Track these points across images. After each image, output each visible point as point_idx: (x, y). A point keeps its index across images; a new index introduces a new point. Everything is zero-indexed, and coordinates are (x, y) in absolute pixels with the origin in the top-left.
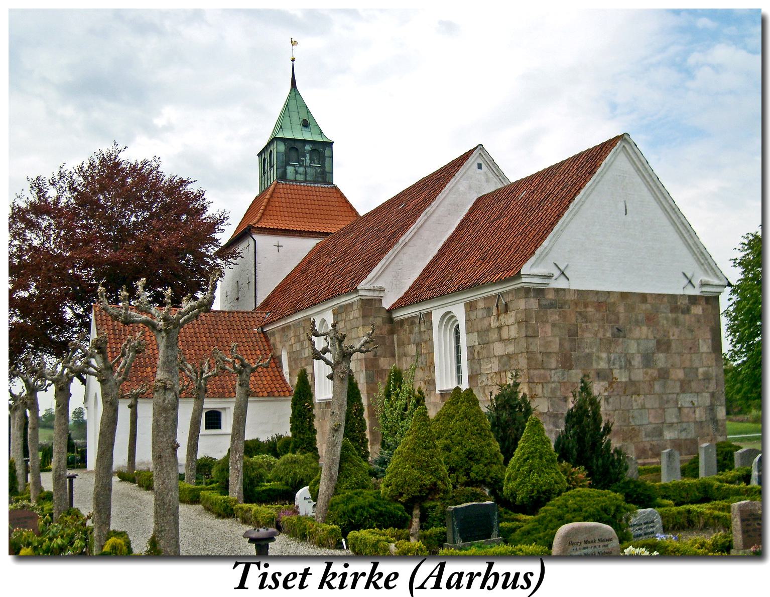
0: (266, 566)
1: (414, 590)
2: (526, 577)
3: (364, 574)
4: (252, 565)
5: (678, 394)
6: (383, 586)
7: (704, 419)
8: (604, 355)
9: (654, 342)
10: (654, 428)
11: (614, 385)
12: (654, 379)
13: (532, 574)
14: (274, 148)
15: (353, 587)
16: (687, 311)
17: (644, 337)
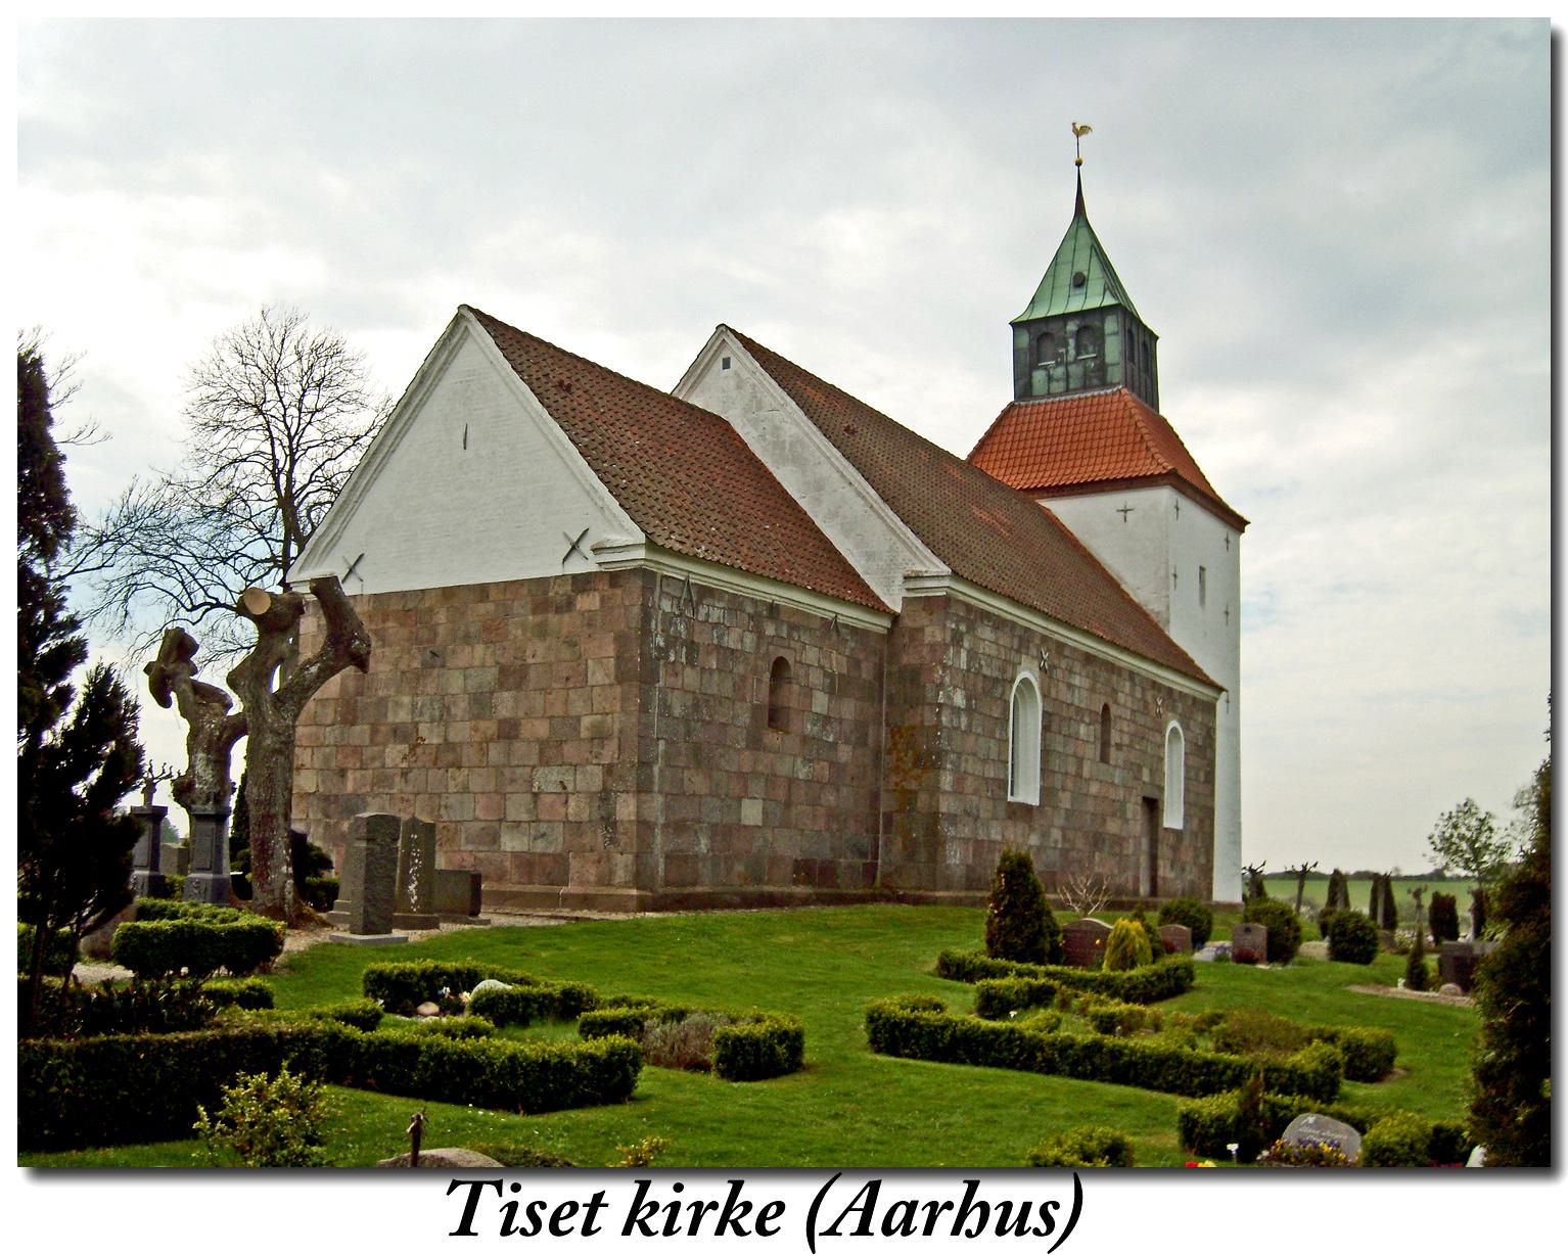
0: (516, 1188)
1: (817, 1238)
2: (1044, 1211)
3: (714, 1205)
4: (485, 1186)
5: (534, 767)
6: (753, 1229)
7: (585, 817)
8: (406, 700)
9: (495, 670)
10: (483, 829)
11: (419, 751)
12: (488, 740)
13: (1056, 1205)
15: (693, 1231)
17: (477, 663)
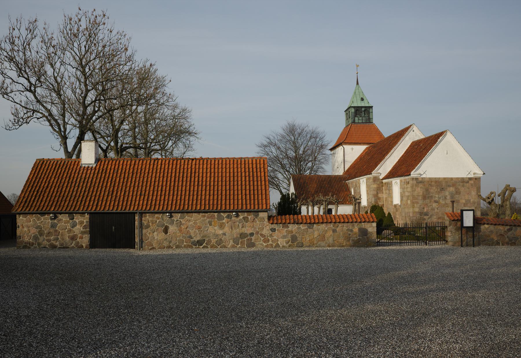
14: (350, 110)
16: (468, 182)
